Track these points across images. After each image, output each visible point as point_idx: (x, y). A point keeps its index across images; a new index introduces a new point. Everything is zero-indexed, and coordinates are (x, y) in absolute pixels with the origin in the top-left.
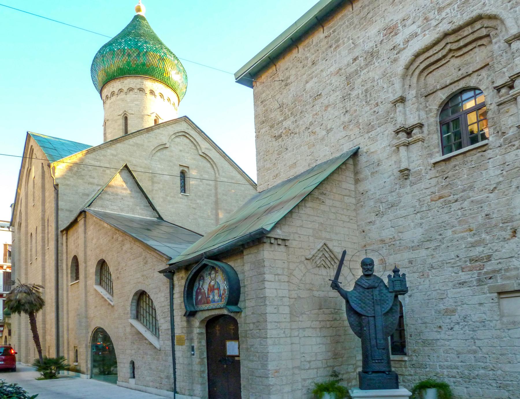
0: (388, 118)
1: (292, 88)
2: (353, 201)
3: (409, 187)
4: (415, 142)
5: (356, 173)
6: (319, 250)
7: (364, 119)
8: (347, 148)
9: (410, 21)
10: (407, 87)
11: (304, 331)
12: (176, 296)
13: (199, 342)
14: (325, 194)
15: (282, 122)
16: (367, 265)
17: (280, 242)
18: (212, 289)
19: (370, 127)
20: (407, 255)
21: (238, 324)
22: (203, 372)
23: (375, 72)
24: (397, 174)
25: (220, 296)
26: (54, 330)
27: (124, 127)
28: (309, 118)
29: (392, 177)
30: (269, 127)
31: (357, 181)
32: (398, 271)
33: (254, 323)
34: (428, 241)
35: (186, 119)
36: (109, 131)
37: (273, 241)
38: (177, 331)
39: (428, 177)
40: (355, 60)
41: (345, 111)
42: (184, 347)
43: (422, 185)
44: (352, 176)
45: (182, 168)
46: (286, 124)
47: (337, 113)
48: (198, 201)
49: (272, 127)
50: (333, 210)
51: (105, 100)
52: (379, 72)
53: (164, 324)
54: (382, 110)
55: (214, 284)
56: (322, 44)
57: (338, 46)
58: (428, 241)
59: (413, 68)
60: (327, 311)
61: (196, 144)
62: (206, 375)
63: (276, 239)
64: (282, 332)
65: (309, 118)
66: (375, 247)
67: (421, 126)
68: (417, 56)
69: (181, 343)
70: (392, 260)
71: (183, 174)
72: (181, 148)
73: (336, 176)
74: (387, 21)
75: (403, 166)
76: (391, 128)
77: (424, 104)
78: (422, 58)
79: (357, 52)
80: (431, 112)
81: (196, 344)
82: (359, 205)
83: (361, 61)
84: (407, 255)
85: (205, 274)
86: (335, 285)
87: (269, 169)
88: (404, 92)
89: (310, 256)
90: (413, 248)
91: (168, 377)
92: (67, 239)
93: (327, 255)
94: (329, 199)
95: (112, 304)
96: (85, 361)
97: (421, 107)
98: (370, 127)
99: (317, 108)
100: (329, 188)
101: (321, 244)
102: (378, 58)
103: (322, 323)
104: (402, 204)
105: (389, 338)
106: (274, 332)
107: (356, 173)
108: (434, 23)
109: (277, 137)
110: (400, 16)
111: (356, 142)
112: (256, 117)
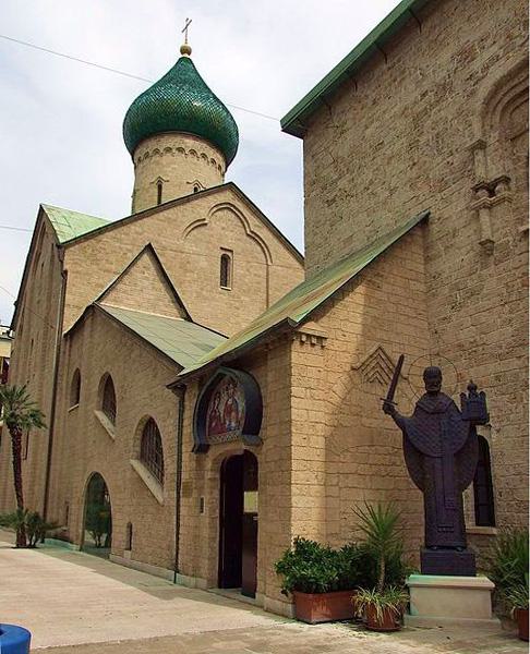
0: (467, 169)
1: (349, 136)
2: (422, 287)
3: (493, 266)
4: (500, 202)
5: (426, 248)
6: (371, 356)
7: (435, 174)
8: (415, 215)
9: (490, 41)
10: (487, 128)
11: (347, 478)
12: (186, 423)
13: (212, 497)
14: (382, 276)
15: (335, 182)
16: (432, 378)
17: (314, 341)
18: (228, 411)
19: (442, 184)
20: (493, 367)
21: (257, 463)
22: (214, 538)
23: (447, 111)
24: (478, 248)
25: (238, 422)
26: (44, 476)
27: (338, 306)
28: (368, 175)
29: (472, 253)
30: (319, 188)
31: (428, 259)
32: (476, 387)
33: (276, 462)
34: (521, 345)
35: (231, 186)
36: (138, 202)
37: (304, 339)
38: (184, 476)
39: (517, 252)
40: (424, 95)
41: (411, 163)
42: (191, 500)
43: (510, 264)
44: (421, 252)
45: (224, 252)
46: (343, 183)
47: (402, 167)
48: (242, 298)
49: (324, 188)
50: (393, 299)
51: (137, 162)
52: (453, 110)
53: (170, 467)
54: (457, 160)
55: (232, 403)
56: (384, 77)
57: (403, 79)
58: (521, 345)
59: (494, 102)
60: (382, 450)
61: (243, 221)
62: (216, 545)
63: (308, 335)
64: (314, 476)
65: (368, 175)
66: (451, 355)
67: (506, 180)
68: (498, 86)
69: (188, 495)
70: (475, 374)
71: (225, 260)
72: (224, 225)
73: (398, 252)
74: (463, 41)
75: (487, 234)
76: (469, 184)
77: (509, 150)
78: (505, 89)
79: (426, 85)
80: (520, 161)
81: (206, 498)
82: (431, 293)
83: (431, 97)
84: (493, 367)
85: (221, 387)
86: (389, 408)
87: (320, 246)
88: (484, 135)
89: (358, 365)
90: (500, 357)
91: (169, 548)
92: (71, 346)
93: (383, 365)
94: (389, 283)
95: (113, 436)
96: (76, 524)
97: (506, 154)
98: (442, 184)
99: (378, 160)
100: (387, 267)
101: (375, 348)
102: (451, 91)
103: (374, 469)
104: (485, 291)
105: (469, 492)
106: (301, 475)
107: (426, 248)
108: (519, 41)
109: (329, 203)
110: (478, 35)
111: (426, 204)
112: (306, 175)
